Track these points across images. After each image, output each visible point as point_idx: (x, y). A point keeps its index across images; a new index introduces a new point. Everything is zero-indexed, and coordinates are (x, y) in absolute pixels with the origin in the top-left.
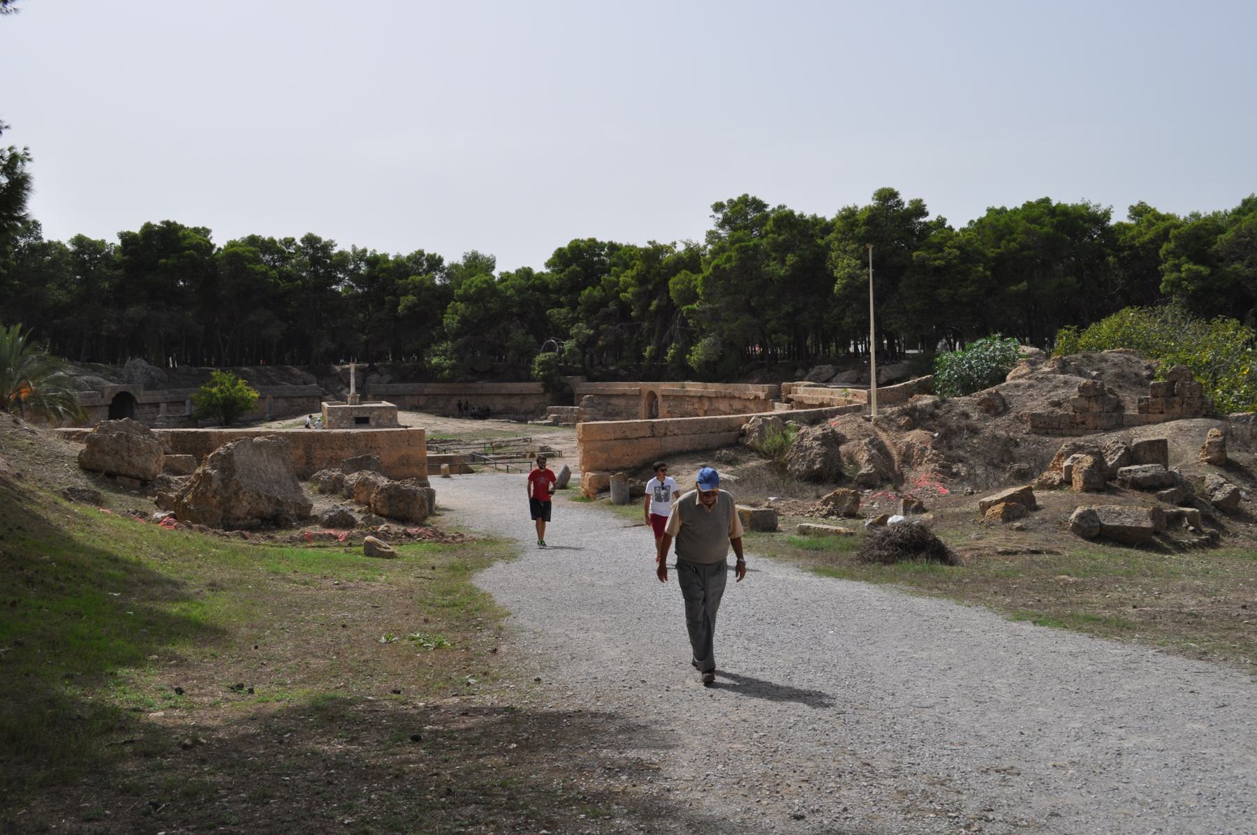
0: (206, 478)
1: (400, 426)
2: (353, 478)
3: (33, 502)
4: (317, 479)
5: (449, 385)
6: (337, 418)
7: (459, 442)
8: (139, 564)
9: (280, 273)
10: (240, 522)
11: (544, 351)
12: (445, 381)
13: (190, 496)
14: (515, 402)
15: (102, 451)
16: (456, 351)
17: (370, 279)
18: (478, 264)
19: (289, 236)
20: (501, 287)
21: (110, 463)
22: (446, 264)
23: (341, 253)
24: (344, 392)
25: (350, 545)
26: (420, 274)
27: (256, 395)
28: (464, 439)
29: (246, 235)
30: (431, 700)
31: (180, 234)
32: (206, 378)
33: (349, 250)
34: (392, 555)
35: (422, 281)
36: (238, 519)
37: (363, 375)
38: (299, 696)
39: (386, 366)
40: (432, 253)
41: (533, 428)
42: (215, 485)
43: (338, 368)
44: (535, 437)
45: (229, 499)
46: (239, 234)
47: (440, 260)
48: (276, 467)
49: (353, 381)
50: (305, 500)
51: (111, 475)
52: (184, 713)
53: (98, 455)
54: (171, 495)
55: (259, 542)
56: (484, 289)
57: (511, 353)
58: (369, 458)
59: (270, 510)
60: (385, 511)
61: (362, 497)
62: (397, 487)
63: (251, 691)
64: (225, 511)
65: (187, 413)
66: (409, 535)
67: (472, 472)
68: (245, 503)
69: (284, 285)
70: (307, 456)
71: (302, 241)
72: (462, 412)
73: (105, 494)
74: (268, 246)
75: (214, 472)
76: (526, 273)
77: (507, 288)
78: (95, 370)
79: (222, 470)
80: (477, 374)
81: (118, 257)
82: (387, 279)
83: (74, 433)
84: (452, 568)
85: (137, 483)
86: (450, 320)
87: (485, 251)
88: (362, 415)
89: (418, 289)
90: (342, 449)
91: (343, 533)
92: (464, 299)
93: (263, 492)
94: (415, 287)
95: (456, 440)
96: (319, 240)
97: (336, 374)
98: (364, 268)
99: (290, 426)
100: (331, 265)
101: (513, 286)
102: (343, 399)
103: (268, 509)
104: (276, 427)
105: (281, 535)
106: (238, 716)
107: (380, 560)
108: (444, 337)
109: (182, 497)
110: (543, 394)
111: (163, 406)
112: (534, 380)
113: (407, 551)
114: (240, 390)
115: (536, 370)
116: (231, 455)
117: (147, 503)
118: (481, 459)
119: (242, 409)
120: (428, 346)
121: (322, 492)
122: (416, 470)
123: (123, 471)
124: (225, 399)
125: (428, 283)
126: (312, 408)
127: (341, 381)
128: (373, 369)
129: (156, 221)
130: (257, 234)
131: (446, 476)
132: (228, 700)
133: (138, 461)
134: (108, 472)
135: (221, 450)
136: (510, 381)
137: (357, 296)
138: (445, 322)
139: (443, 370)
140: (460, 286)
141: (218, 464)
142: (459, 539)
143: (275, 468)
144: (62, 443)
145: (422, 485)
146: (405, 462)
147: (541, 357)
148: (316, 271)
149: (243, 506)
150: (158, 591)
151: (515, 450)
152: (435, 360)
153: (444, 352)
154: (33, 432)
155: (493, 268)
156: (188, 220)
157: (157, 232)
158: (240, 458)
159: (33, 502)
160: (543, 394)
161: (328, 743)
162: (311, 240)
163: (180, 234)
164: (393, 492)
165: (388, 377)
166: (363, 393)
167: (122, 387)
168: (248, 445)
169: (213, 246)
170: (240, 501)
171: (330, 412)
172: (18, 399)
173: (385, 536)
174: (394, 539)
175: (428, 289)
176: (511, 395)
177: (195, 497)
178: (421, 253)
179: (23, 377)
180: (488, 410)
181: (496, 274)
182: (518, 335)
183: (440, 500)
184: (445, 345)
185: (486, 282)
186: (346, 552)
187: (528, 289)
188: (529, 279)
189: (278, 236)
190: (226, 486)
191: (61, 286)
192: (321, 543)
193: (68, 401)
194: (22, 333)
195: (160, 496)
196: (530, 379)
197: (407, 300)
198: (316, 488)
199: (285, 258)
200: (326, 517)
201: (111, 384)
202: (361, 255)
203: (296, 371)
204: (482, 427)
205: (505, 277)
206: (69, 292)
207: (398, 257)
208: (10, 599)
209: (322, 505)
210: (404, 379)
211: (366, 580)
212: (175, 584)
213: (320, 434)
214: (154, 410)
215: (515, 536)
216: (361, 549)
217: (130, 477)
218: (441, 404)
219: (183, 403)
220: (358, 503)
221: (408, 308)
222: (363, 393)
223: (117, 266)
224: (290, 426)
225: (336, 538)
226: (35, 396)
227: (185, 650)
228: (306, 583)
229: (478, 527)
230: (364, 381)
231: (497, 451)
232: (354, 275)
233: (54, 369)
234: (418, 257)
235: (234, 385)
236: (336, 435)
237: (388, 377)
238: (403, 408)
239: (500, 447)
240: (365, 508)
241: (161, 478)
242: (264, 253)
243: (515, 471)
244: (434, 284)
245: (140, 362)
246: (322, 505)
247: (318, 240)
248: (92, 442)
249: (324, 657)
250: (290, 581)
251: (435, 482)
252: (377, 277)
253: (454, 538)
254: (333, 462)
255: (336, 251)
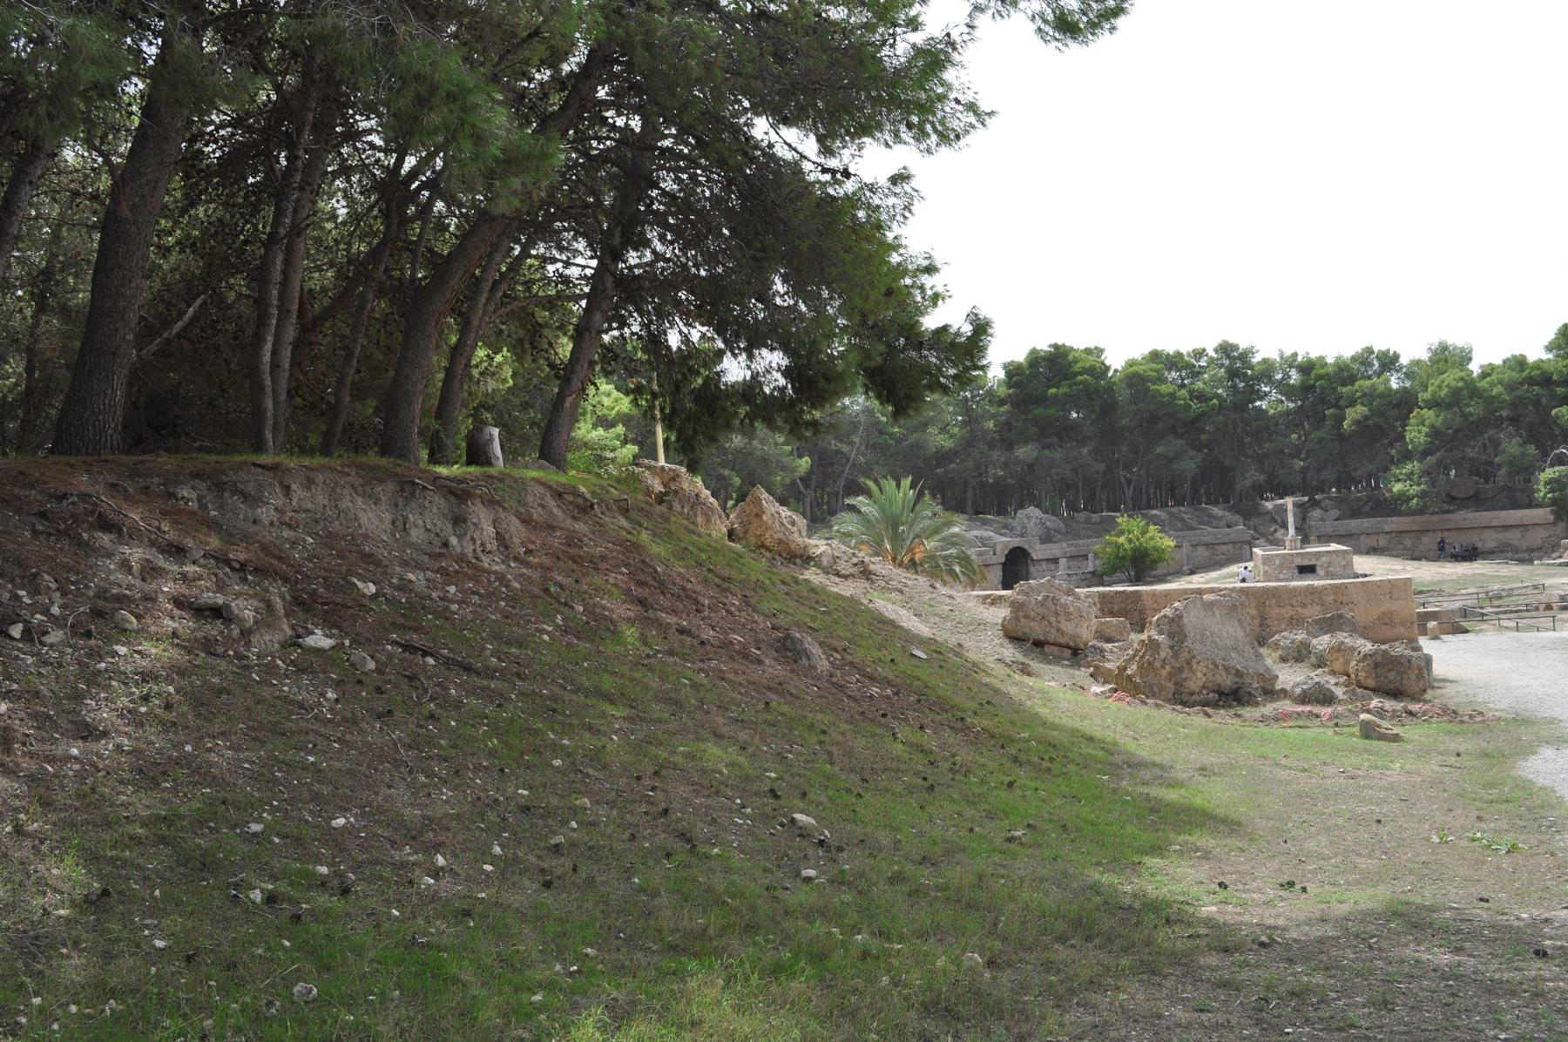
0: (1153, 645)
1: (1357, 576)
2: (1323, 642)
3: (988, 675)
4: (1276, 644)
5: (1418, 518)
6: (1275, 568)
7: (1440, 593)
8: (1115, 744)
9: (1191, 393)
10: (1195, 697)
11: (1552, 465)
12: (1413, 513)
13: (1135, 667)
14: (1514, 536)
15: (1027, 617)
16: (1427, 472)
17: (1306, 389)
18: (1447, 357)
19: (1199, 346)
20: (1484, 384)
21: (1036, 630)
22: (1404, 361)
23: (1265, 361)
24: (1279, 535)
25: (1337, 725)
26: (1369, 377)
27: (1172, 544)
28: (1447, 588)
29: (1146, 350)
30: (1535, 912)
31: (1071, 357)
32: (1110, 526)
33: (1275, 356)
34: (1396, 738)
35: (1373, 388)
36: (1192, 694)
37: (1302, 509)
38: (1366, 898)
39: (1330, 499)
40: (1384, 348)
41: (1542, 570)
42: (1164, 652)
43: (1269, 505)
44: (1548, 582)
45: (1180, 670)
46: (1138, 351)
47: (1396, 357)
48: (1231, 630)
49: (1291, 520)
50: (1268, 670)
51: (1038, 644)
52: (1238, 910)
53: (1023, 621)
54: (1109, 666)
55: (1223, 719)
56: (1461, 389)
57: (1503, 471)
58: (1340, 616)
59: (1228, 682)
60: (1371, 683)
61: (1337, 666)
62: (1385, 652)
63: (1304, 890)
64: (1176, 684)
65: (1090, 569)
66: (1411, 713)
67: (1466, 631)
68: (1199, 675)
69: (1196, 406)
70: (1261, 614)
71: (1216, 351)
72: (1445, 553)
73: (1035, 665)
74: (1173, 361)
75: (1161, 638)
76: (1519, 362)
77: (1492, 385)
78: (984, 523)
79: (1171, 636)
80: (1455, 501)
81: (1003, 392)
82: (1322, 387)
83: (987, 597)
84: (1484, 755)
85: (1068, 653)
86: (1416, 434)
87: (1456, 340)
88: (1306, 562)
89: (1368, 397)
90: (1304, 606)
91: (1326, 711)
92: (1434, 404)
93: (1220, 662)
94: (1365, 395)
95: (1436, 591)
96: (1236, 347)
97: (1268, 513)
98: (1295, 377)
99: (1216, 580)
100: (1253, 378)
101: (1500, 382)
102: (1278, 543)
103: (1227, 682)
104: (1197, 581)
105: (1247, 711)
106: (1302, 917)
107: (1382, 744)
108: (1407, 456)
109: (1125, 668)
110: (1554, 524)
111: (1063, 562)
112: (1538, 506)
113: (1413, 732)
114: (1152, 538)
115: (1542, 492)
116: (1180, 617)
117: (1082, 674)
118: (1474, 614)
119: (1155, 562)
120: (1386, 470)
121: (1284, 660)
122: (1402, 631)
123: (1051, 639)
124: (1134, 550)
125: (1381, 388)
126: (1239, 553)
127: (1273, 520)
128: (1314, 504)
129: (1043, 346)
130: (1159, 348)
131: (1435, 638)
132: (1282, 899)
133: (1068, 627)
134: (1036, 641)
135: (1168, 611)
136: (1503, 508)
137: (1288, 413)
138: (1408, 436)
139: (1410, 499)
140: (1425, 388)
141: (1166, 628)
142: (1479, 719)
143: (1231, 632)
144: (981, 608)
145: (1414, 649)
146: (1387, 620)
147: (1549, 473)
148: (1234, 386)
149: (1196, 680)
150: (1145, 774)
151: (1522, 600)
152: (1397, 487)
153: (1410, 476)
154: (951, 597)
155: (1470, 359)
156: (1077, 341)
157: (1044, 359)
158: (1190, 621)
159: (988, 675)
160: (1554, 524)
161: (1428, 950)
162: (1226, 349)
163: (1071, 357)
164: (1379, 659)
165: (1335, 513)
166: (1305, 535)
167: (1016, 542)
168: (1199, 604)
169: (1108, 368)
170: (1194, 673)
171: (1266, 560)
172: (912, 560)
173: (1380, 713)
174: (1392, 718)
175: (1382, 396)
176: (1506, 528)
177: (1140, 667)
178: (1369, 351)
179: (917, 536)
180: (1475, 549)
181: (1475, 367)
182: (1512, 446)
183: (1438, 669)
184: (1409, 467)
185: (1462, 379)
186: (1336, 733)
187: (1521, 384)
188: (1522, 371)
189: (1186, 348)
190: (1176, 655)
191: (943, 430)
192: (1301, 723)
193: (964, 559)
194: (913, 486)
195: (1096, 667)
196: (1531, 504)
197: (1354, 413)
198: (1276, 655)
199: (1195, 374)
200: (1298, 691)
201: (1004, 539)
202: (1291, 361)
203: (1216, 511)
204: (1469, 572)
205: (1488, 371)
206: (952, 436)
207: (1339, 358)
208: (1007, 779)
209: (1290, 677)
210: (1356, 513)
211: (1377, 767)
212: (1161, 767)
213: (1276, 588)
214: (1052, 566)
215: (1555, 715)
216: (1356, 730)
217: (1060, 645)
218: (1408, 543)
219: (1085, 557)
220: (1333, 673)
221: (1357, 422)
222: (1305, 535)
223: (1002, 402)
224: (1216, 580)
225: (1318, 716)
226: (931, 558)
227: (1205, 841)
228: (1305, 770)
229: (1499, 703)
230: (1304, 519)
231: (1496, 603)
232: (1283, 386)
233: (949, 524)
234: (1365, 357)
235: (1144, 532)
236: (1295, 589)
237: (1335, 513)
238: (1358, 552)
239: (1500, 598)
240: (1343, 679)
241: (1094, 647)
242: (1170, 370)
243: (1528, 628)
244: (1390, 389)
245: (1033, 511)
246: (1290, 677)
247: (1234, 347)
248: (1017, 607)
249: (1370, 857)
250: (1285, 767)
251: (1424, 642)
252: (1313, 386)
253: (1471, 717)
254: (1295, 622)
255: (1257, 359)
